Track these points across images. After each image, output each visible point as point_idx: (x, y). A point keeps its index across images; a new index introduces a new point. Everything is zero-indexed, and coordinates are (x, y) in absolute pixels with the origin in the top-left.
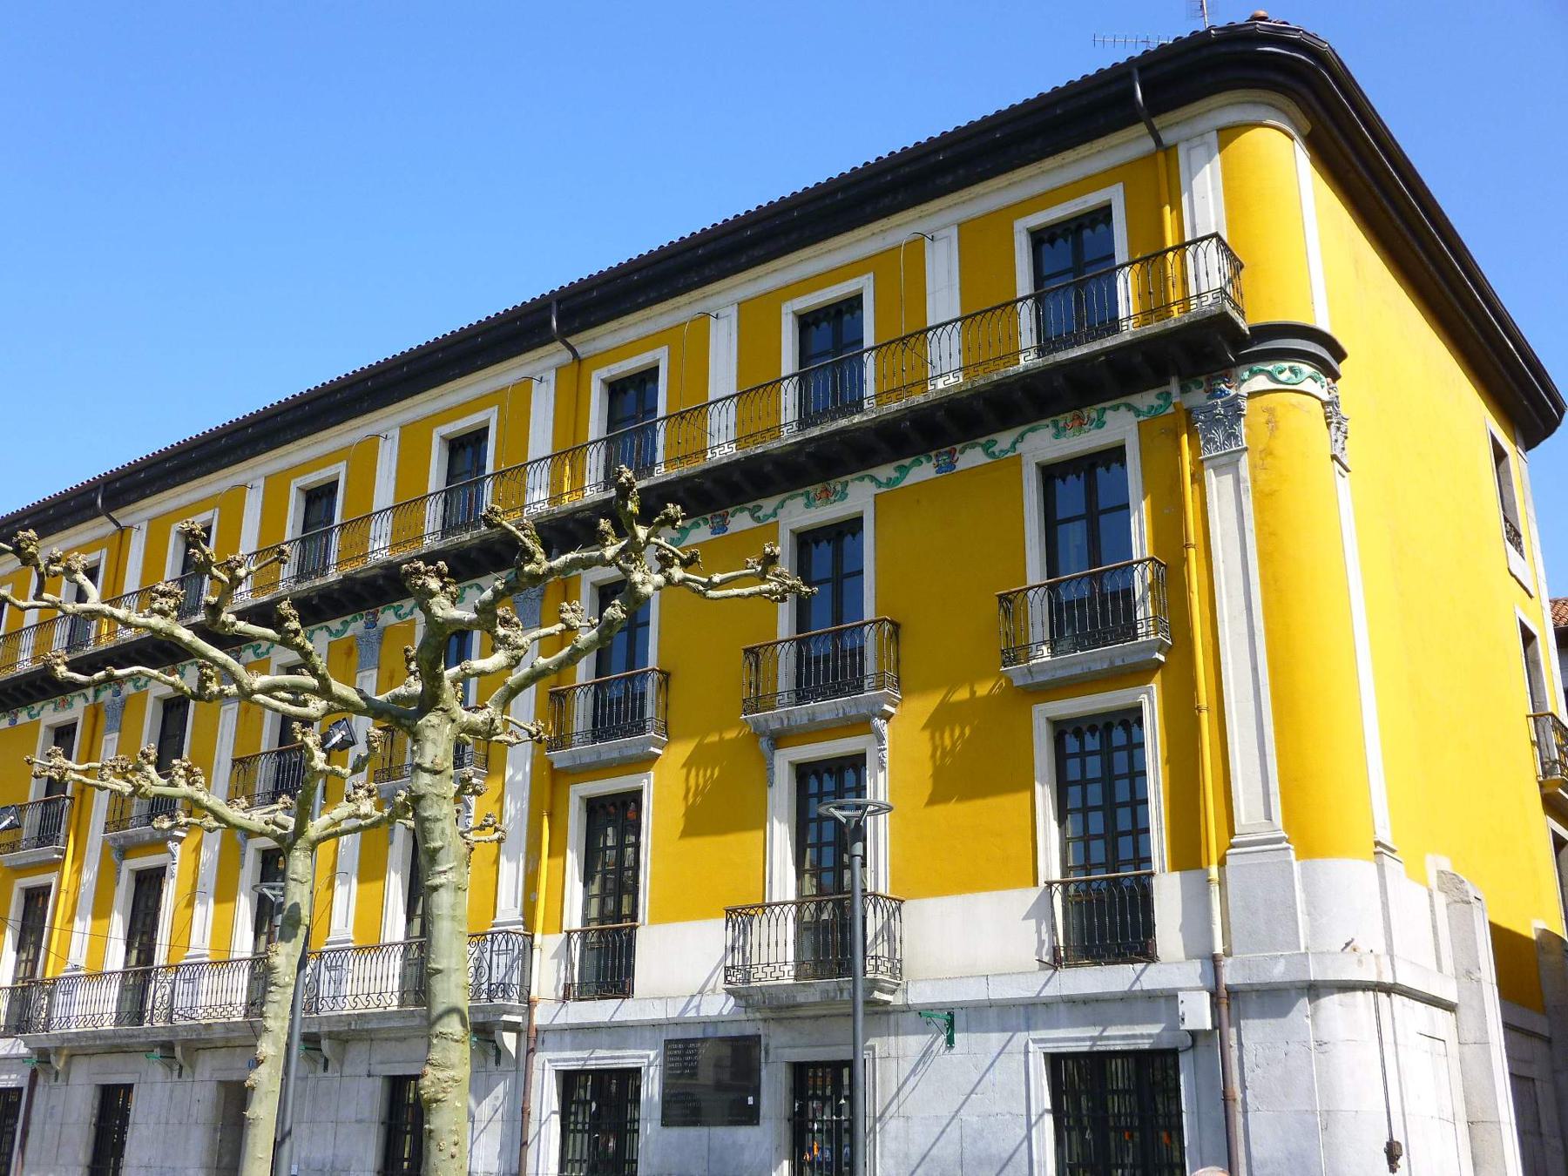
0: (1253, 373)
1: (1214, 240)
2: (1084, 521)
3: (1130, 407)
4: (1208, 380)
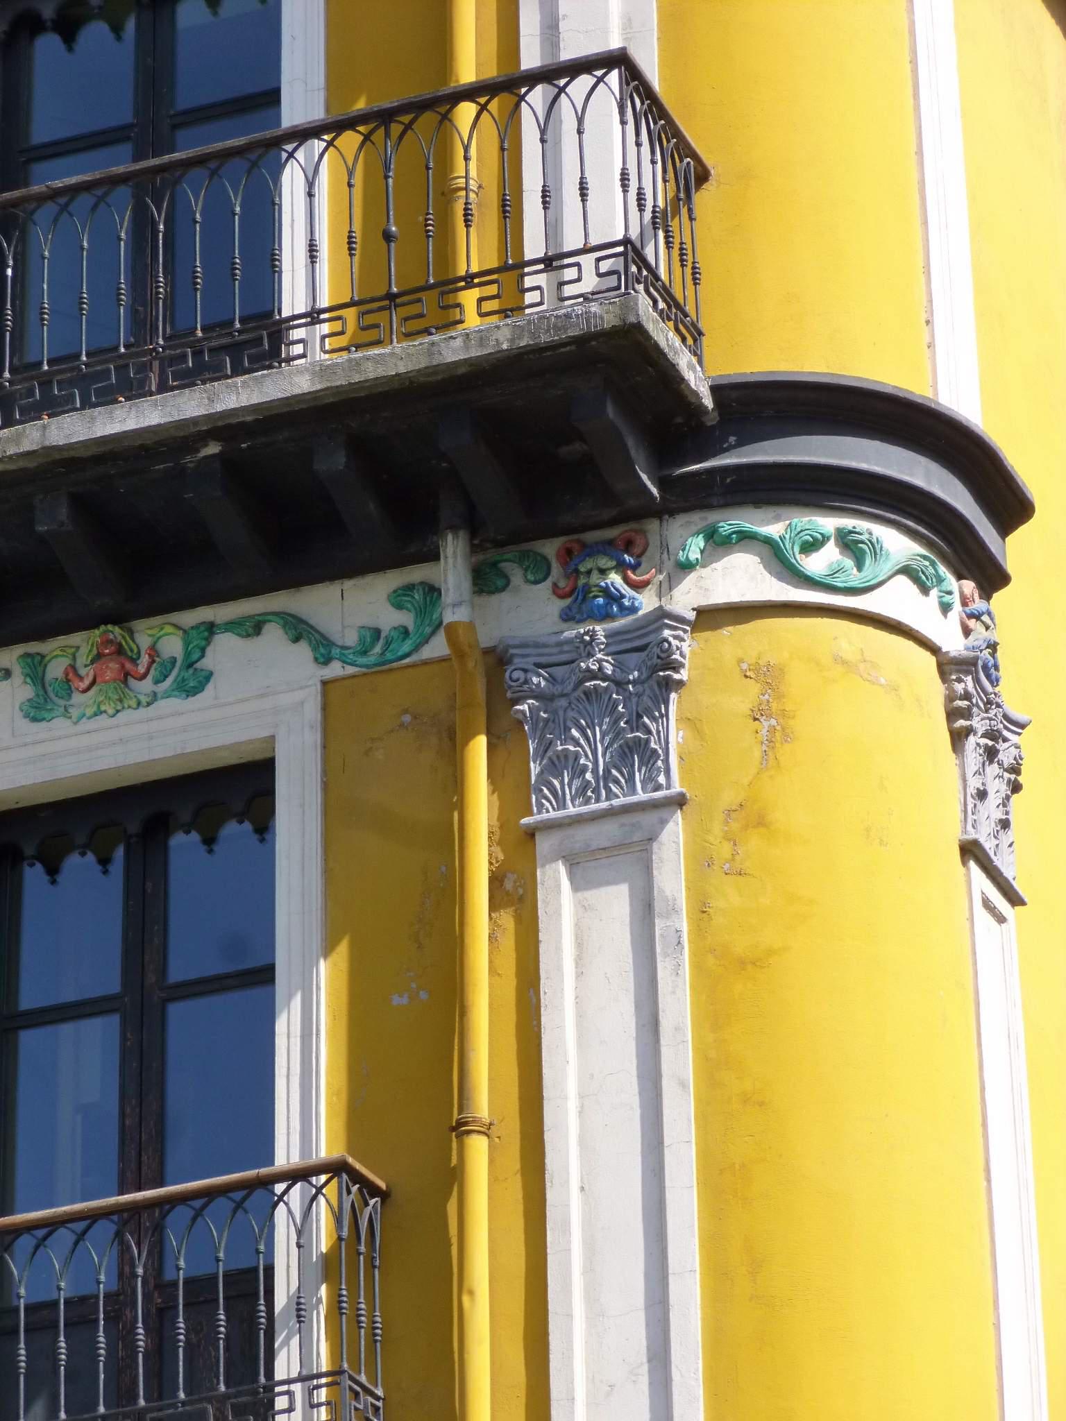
0: (719, 544)
1: (614, 77)
2: (114, 1021)
3: (298, 629)
4: (567, 555)
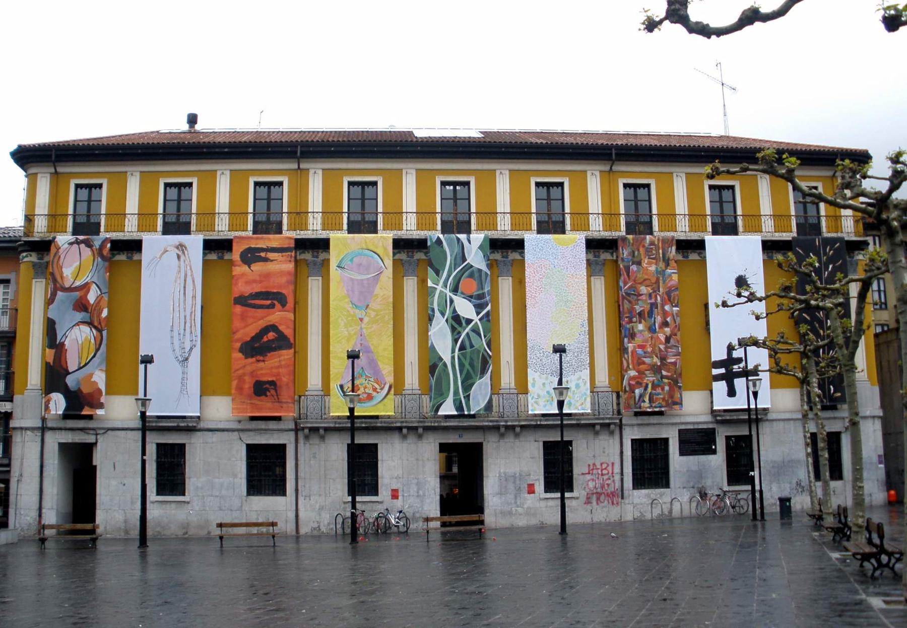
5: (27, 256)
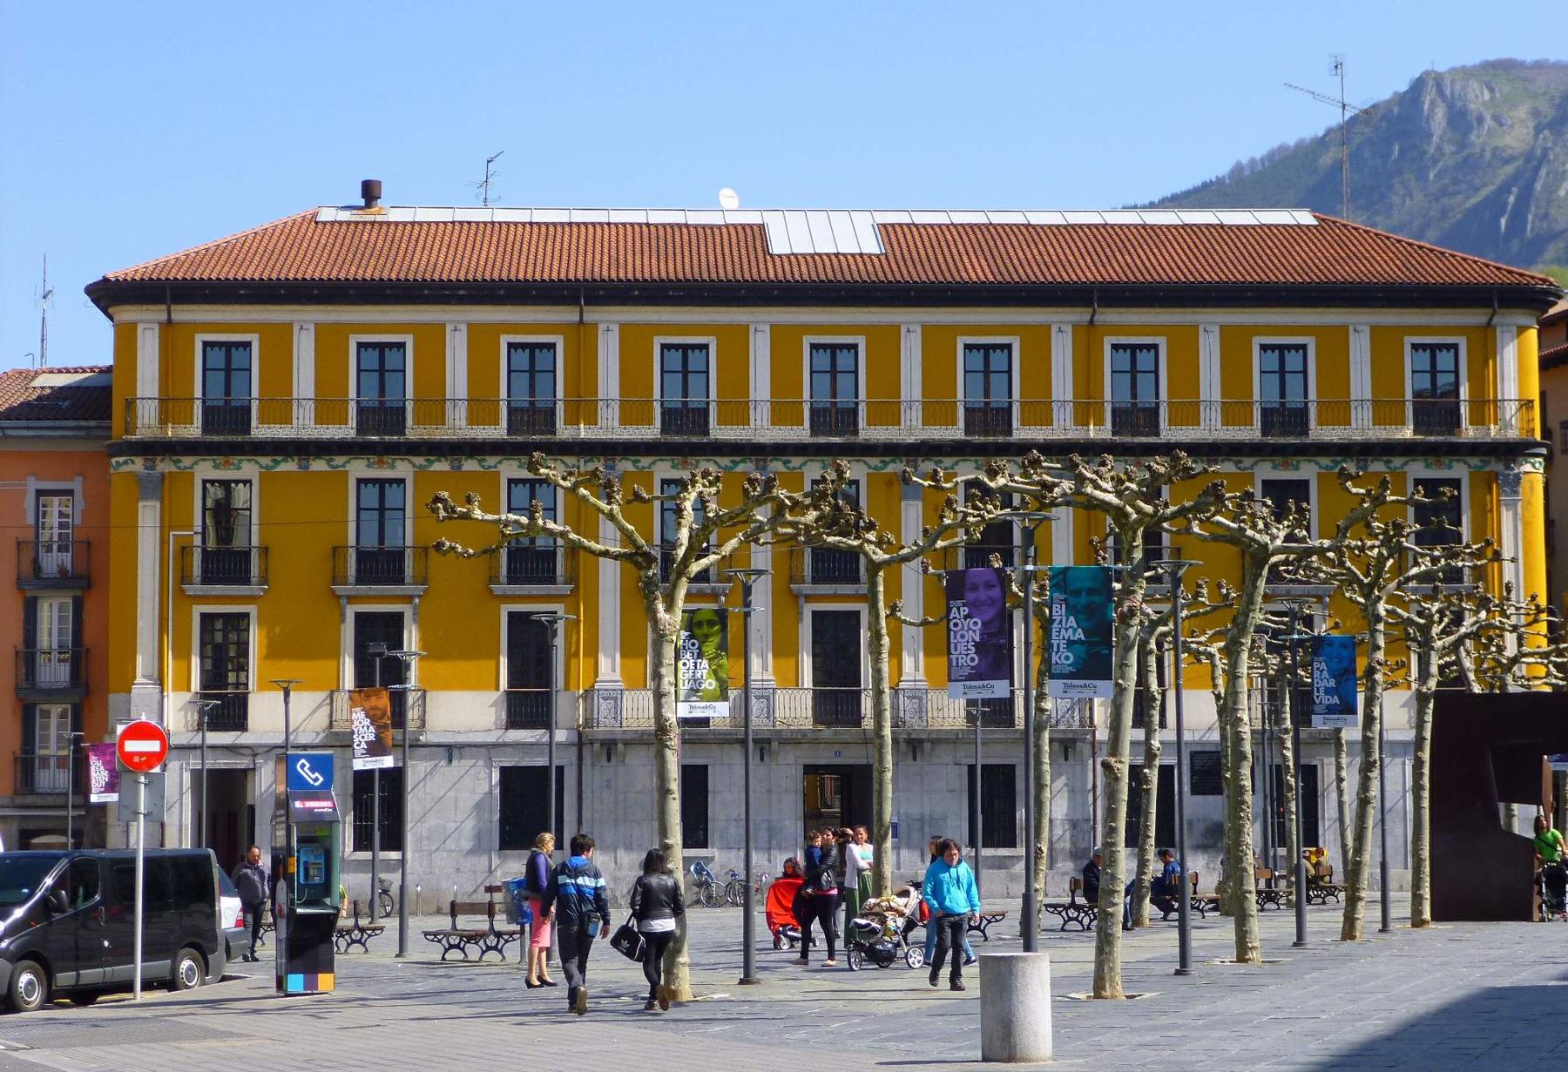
3: (1466, 463)
5: (125, 463)
